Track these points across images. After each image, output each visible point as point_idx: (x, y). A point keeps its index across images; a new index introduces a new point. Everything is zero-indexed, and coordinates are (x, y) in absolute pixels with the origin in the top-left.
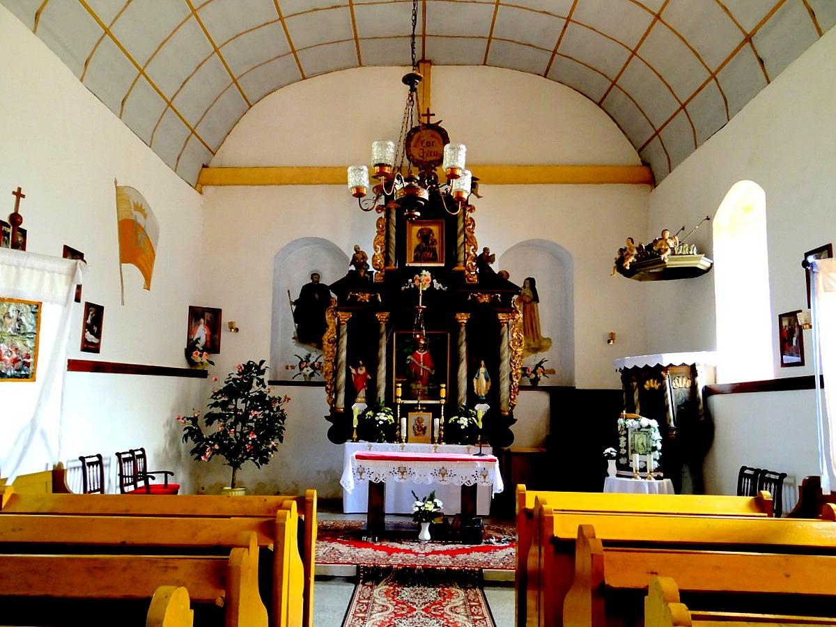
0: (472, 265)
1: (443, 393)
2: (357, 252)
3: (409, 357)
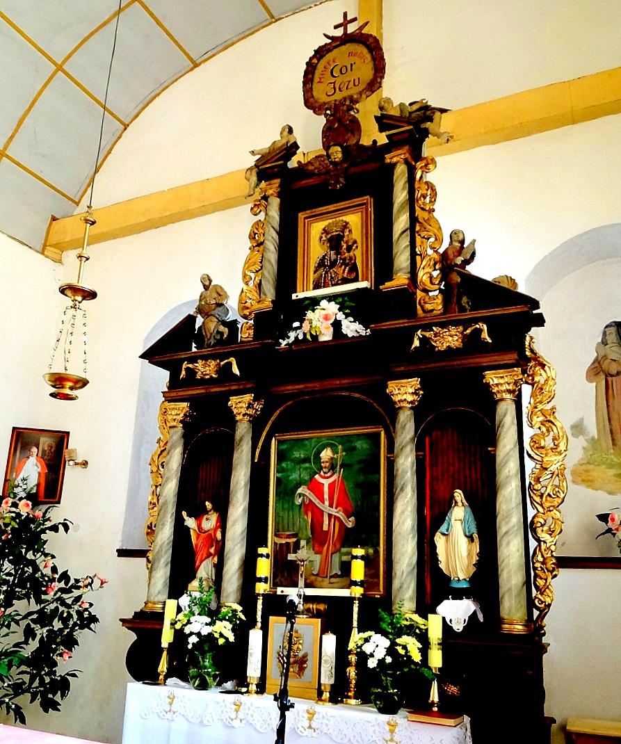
0: (431, 277)
1: (358, 571)
2: (206, 288)
3: (300, 491)
